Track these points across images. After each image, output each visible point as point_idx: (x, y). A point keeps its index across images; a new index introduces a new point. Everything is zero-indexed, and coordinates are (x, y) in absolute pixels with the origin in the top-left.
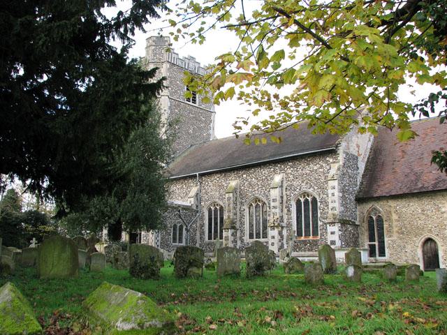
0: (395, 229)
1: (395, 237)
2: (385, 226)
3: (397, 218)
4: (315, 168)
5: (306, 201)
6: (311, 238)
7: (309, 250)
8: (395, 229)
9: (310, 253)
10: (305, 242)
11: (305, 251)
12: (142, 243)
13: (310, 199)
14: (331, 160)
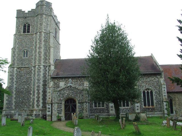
0: (177, 104)
1: (177, 106)
2: (173, 102)
3: (178, 99)
4: (152, 79)
5: (148, 92)
6: (151, 107)
7: (151, 112)
8: (177, 104)
9: (151, 113)
10: (149, 109)
11: (149, 112)
12: (136, 104)
13: (149, 91)
14: (159, 77)
